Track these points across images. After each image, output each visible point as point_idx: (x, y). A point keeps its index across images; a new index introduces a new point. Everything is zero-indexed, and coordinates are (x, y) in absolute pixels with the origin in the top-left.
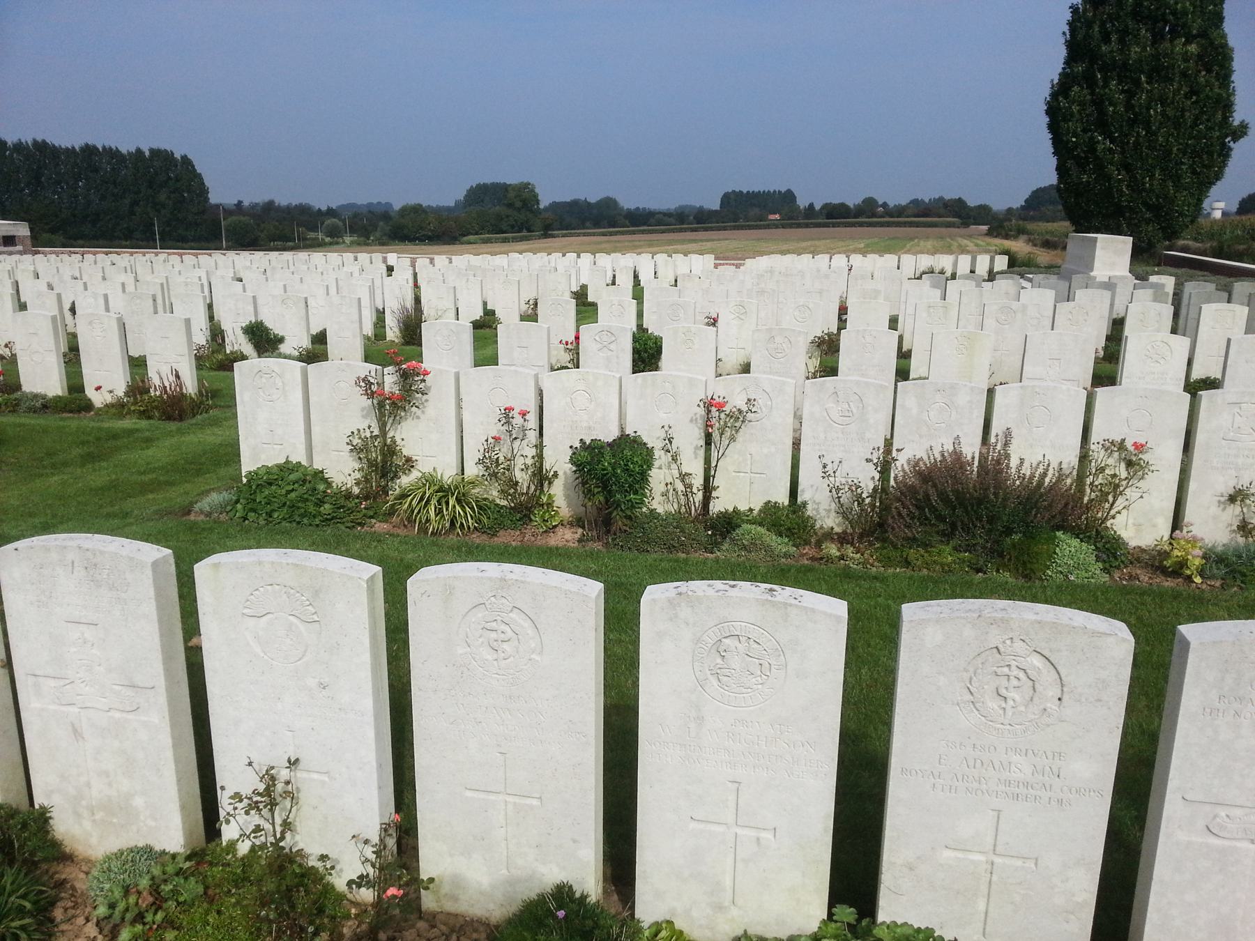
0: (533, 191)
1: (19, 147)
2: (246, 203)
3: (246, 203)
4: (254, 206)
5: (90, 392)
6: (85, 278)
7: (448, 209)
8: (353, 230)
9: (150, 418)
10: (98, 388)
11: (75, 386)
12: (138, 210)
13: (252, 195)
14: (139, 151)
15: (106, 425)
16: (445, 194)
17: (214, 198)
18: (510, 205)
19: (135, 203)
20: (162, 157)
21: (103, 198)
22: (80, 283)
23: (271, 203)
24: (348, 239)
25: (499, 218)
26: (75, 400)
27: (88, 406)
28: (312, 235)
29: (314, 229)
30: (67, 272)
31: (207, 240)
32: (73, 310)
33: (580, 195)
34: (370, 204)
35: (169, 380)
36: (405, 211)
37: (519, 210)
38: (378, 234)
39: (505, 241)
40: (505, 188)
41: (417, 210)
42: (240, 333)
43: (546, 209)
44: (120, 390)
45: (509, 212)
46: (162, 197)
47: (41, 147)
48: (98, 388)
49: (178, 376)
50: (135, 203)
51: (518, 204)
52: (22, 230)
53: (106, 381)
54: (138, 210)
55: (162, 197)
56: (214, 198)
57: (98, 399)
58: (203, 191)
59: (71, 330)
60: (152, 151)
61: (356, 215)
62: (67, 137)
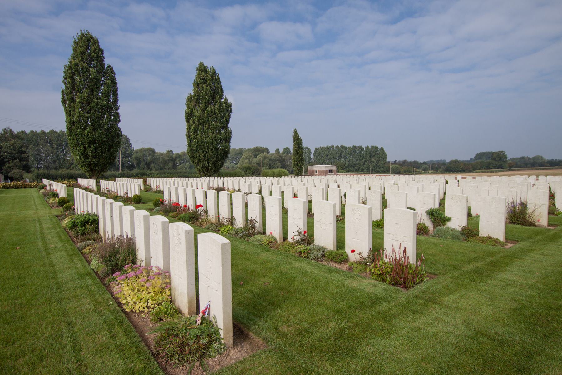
0: (504, 154)
1: (337, 147)
2: (397, 161)
3: (397, 161)
4: (400, 162)
5: (348, 250)
6: (351, 183)
7: (467, 161)
8: (432, 169)
9: (384, 281)
10: (353, 251)
11: (340, 243)
12: (366, 163)
13: (399, 159)
14: (368, 146)
15: (354, 284)
16: (466, 155)
17: (388, 160)
18: (495, 159)
19: (366, 161)
20: (375, 148)
21: (357, 160)
22: (349, 185)
23: (405, 160)
24: (430, 171)
25: (489, 164)
26: (339, 254)
27: (346, 260)
28: (418, 170)
29: (419, 168)
30: (345, 181)
31: (385, 172)
32: (345, 195)
33: (525, 155)
34: (438, 160)
35: (399, 254)
36: (451, 162)
37: (498, 161)
38: (441, 170)
39: (492, 172)
40: (493, 153)
41: (456, 162)
42: (424, 213)
43: (509, 160)
44: (365, 254)
45: (494, 161)
46: (373, 159)
47: (342, 147)
48: (353, 251)
49: (405, 251)
50: (366, 161)
51: (498, 159)
52: (334, 168)
53: (358, 244)
54: (366, 163)
55: (373, 159)
56: (388, 160)
57: (353, 257)
58: (386, 157)
59: (343, 203)
60: (109, 66)
61: (433, 164)
62: (348, 144)
